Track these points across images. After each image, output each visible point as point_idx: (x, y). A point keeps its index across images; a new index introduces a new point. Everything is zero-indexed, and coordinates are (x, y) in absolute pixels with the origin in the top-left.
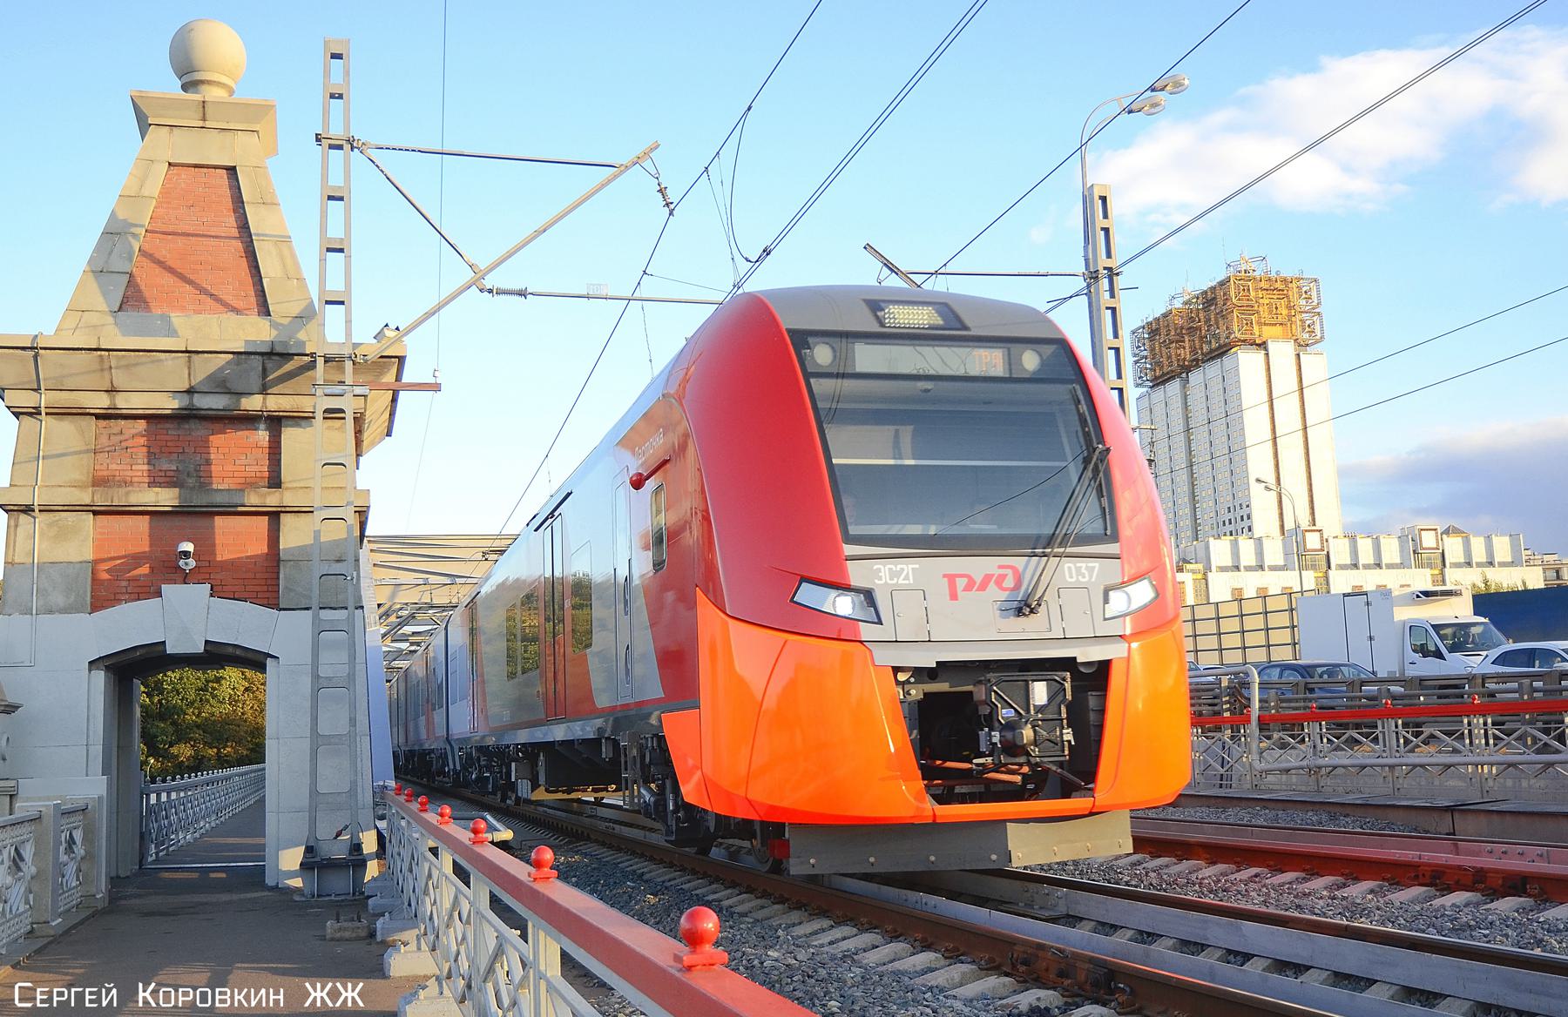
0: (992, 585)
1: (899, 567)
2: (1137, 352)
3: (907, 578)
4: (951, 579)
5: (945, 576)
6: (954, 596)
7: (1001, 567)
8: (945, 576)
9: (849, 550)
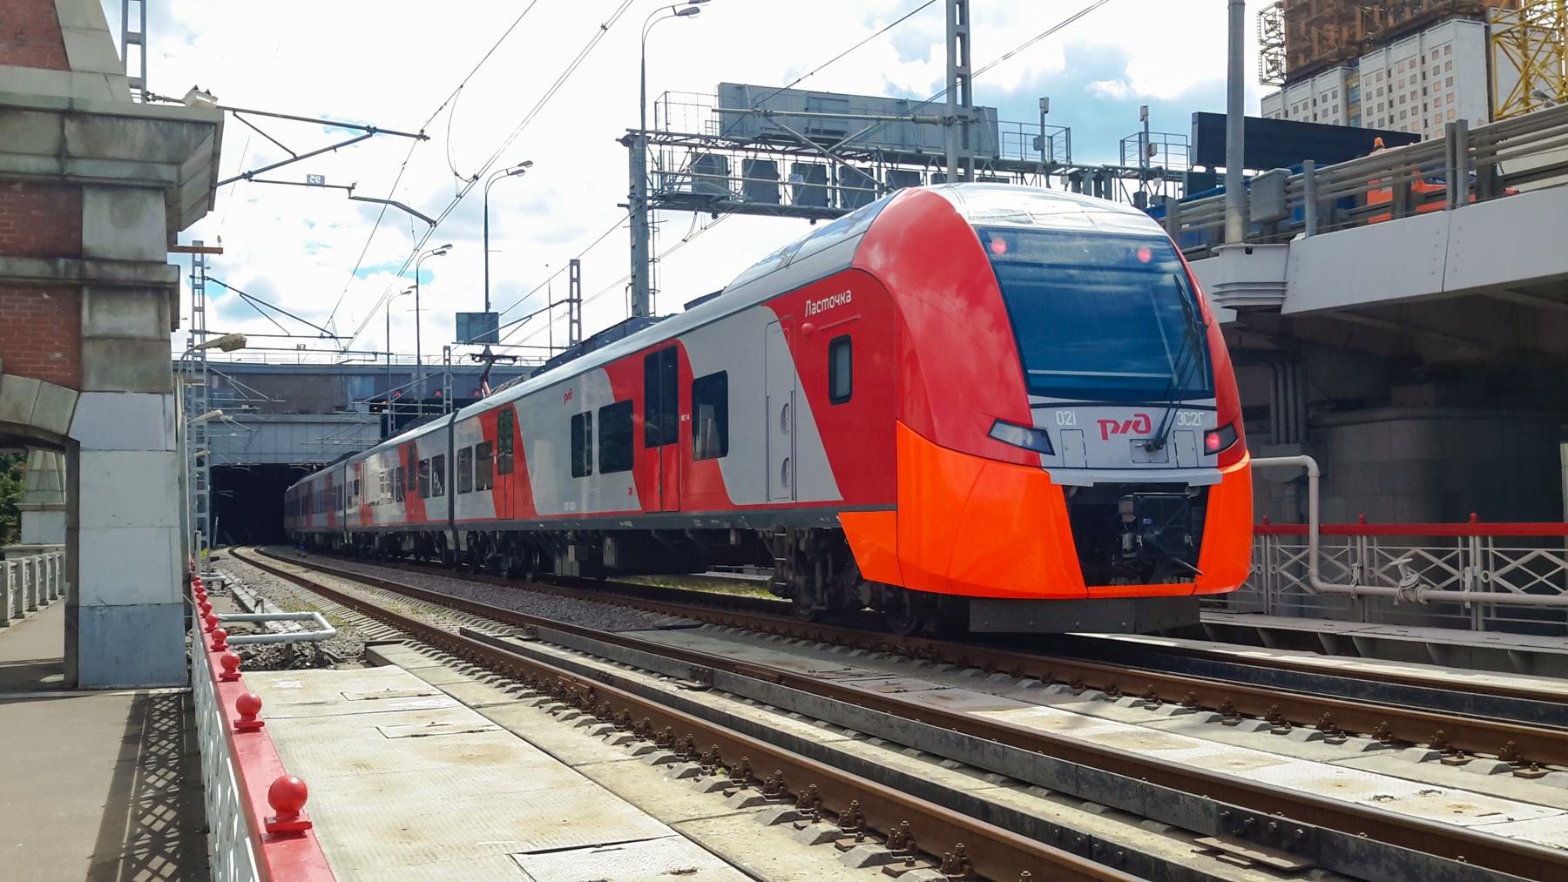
0: (1131, 429)
1: (1192, 413)
2: (1264, 37)
3: (1071, 421)
4: (1103, 423)
5: (1099, 421)
6: (1105, 437)
7: (1136, 415)
8: (1099, 421)
9: (1033, 399)
